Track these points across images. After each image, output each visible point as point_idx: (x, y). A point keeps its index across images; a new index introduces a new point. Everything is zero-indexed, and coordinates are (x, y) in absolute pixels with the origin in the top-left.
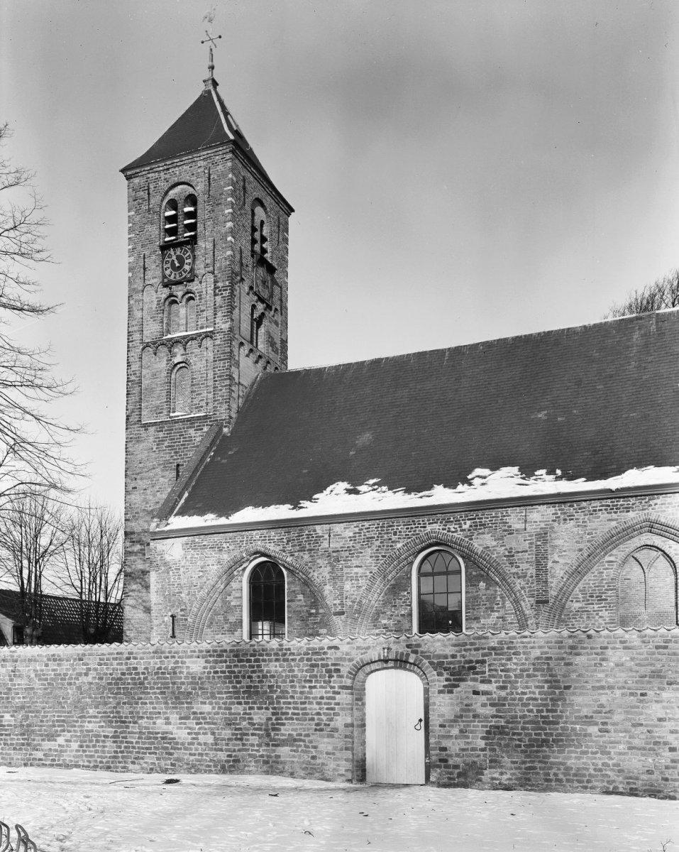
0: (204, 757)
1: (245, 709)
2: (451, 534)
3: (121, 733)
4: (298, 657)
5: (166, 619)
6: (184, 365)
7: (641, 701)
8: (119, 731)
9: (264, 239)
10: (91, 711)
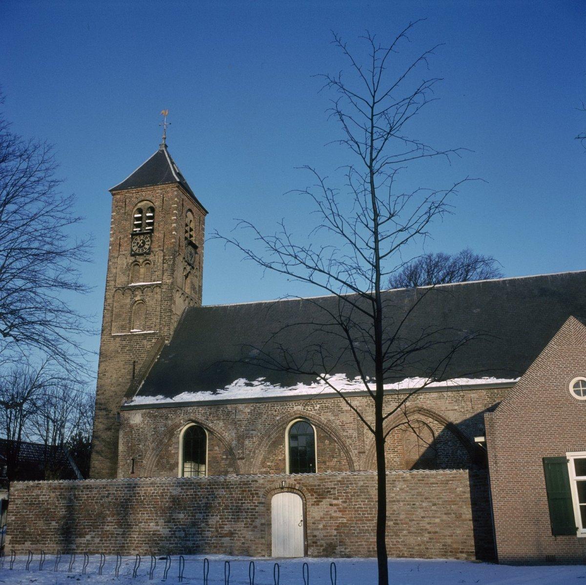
0: (179, 545)
1: (204, 516)
2: (308, 412)
3: (127, 532)
4: (235, 487)
5: (128, 461)
6: (141, 301)
7: (413, 508)
8: (126, 530)
9: (191, 230)
10: (109, 519)
